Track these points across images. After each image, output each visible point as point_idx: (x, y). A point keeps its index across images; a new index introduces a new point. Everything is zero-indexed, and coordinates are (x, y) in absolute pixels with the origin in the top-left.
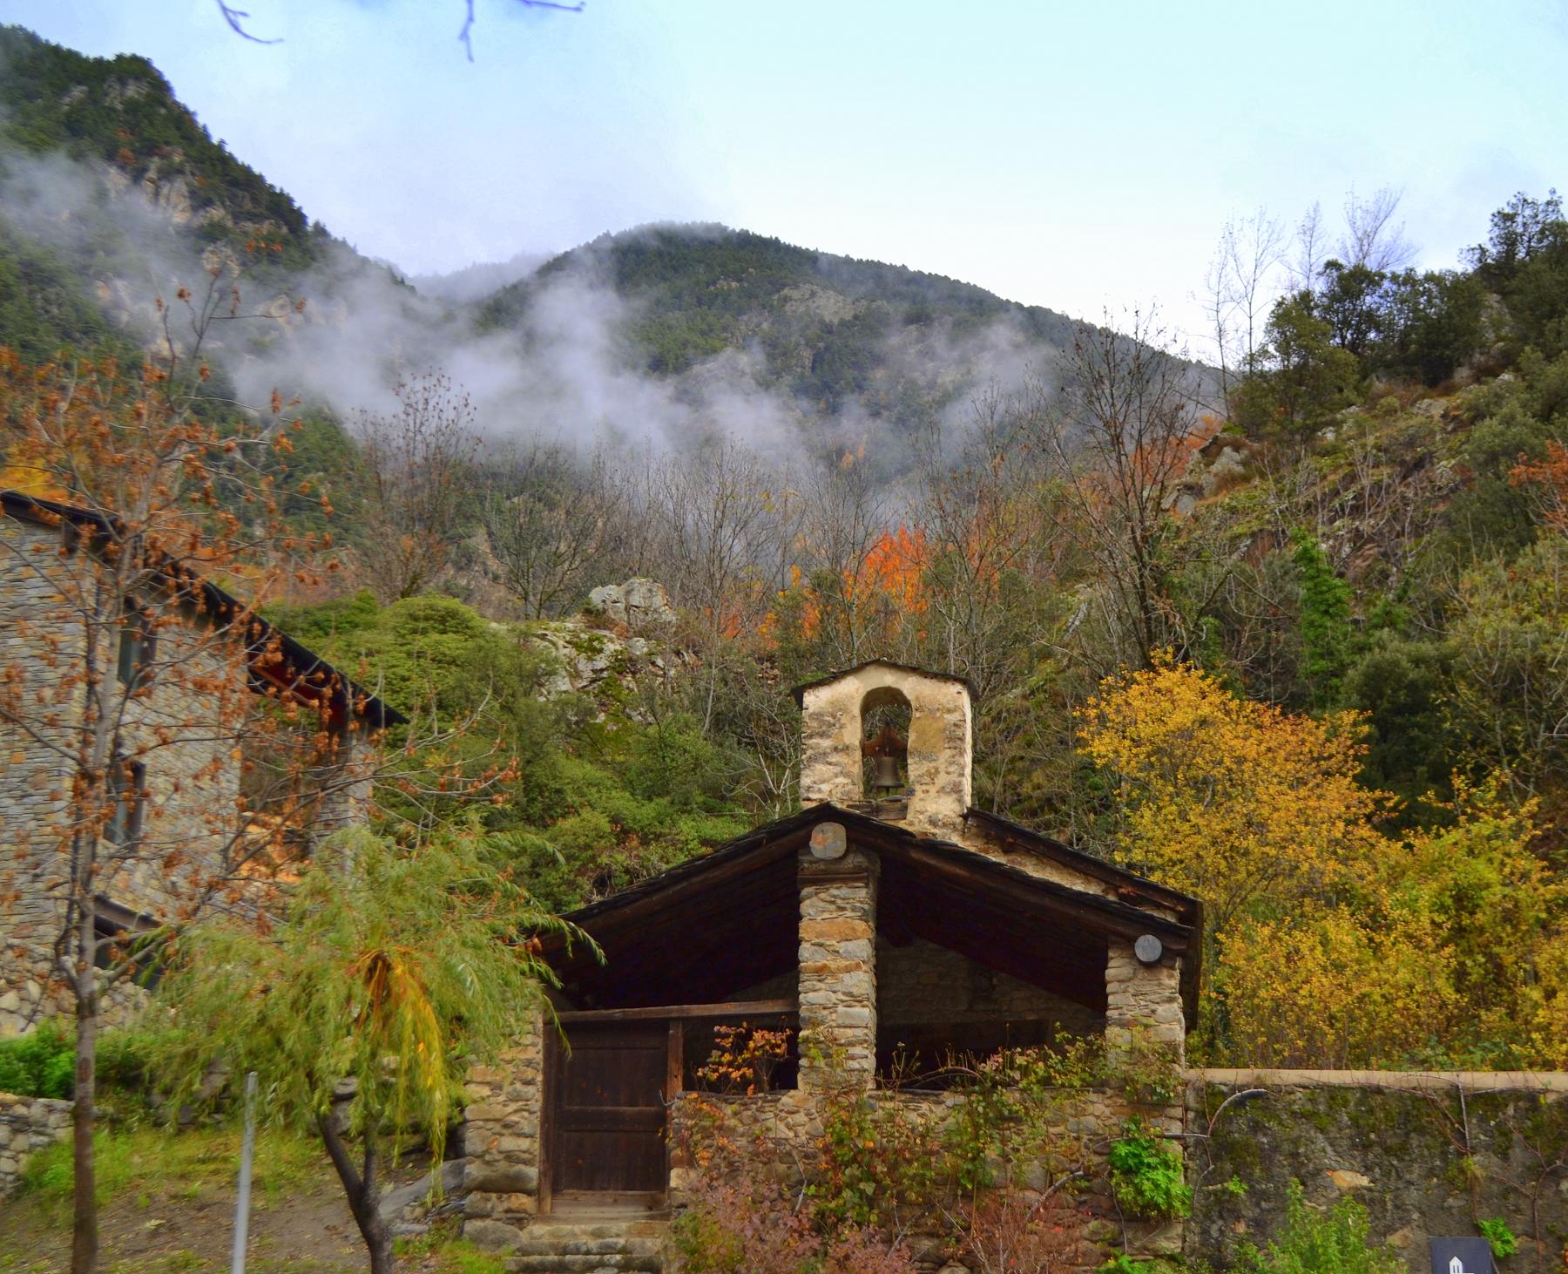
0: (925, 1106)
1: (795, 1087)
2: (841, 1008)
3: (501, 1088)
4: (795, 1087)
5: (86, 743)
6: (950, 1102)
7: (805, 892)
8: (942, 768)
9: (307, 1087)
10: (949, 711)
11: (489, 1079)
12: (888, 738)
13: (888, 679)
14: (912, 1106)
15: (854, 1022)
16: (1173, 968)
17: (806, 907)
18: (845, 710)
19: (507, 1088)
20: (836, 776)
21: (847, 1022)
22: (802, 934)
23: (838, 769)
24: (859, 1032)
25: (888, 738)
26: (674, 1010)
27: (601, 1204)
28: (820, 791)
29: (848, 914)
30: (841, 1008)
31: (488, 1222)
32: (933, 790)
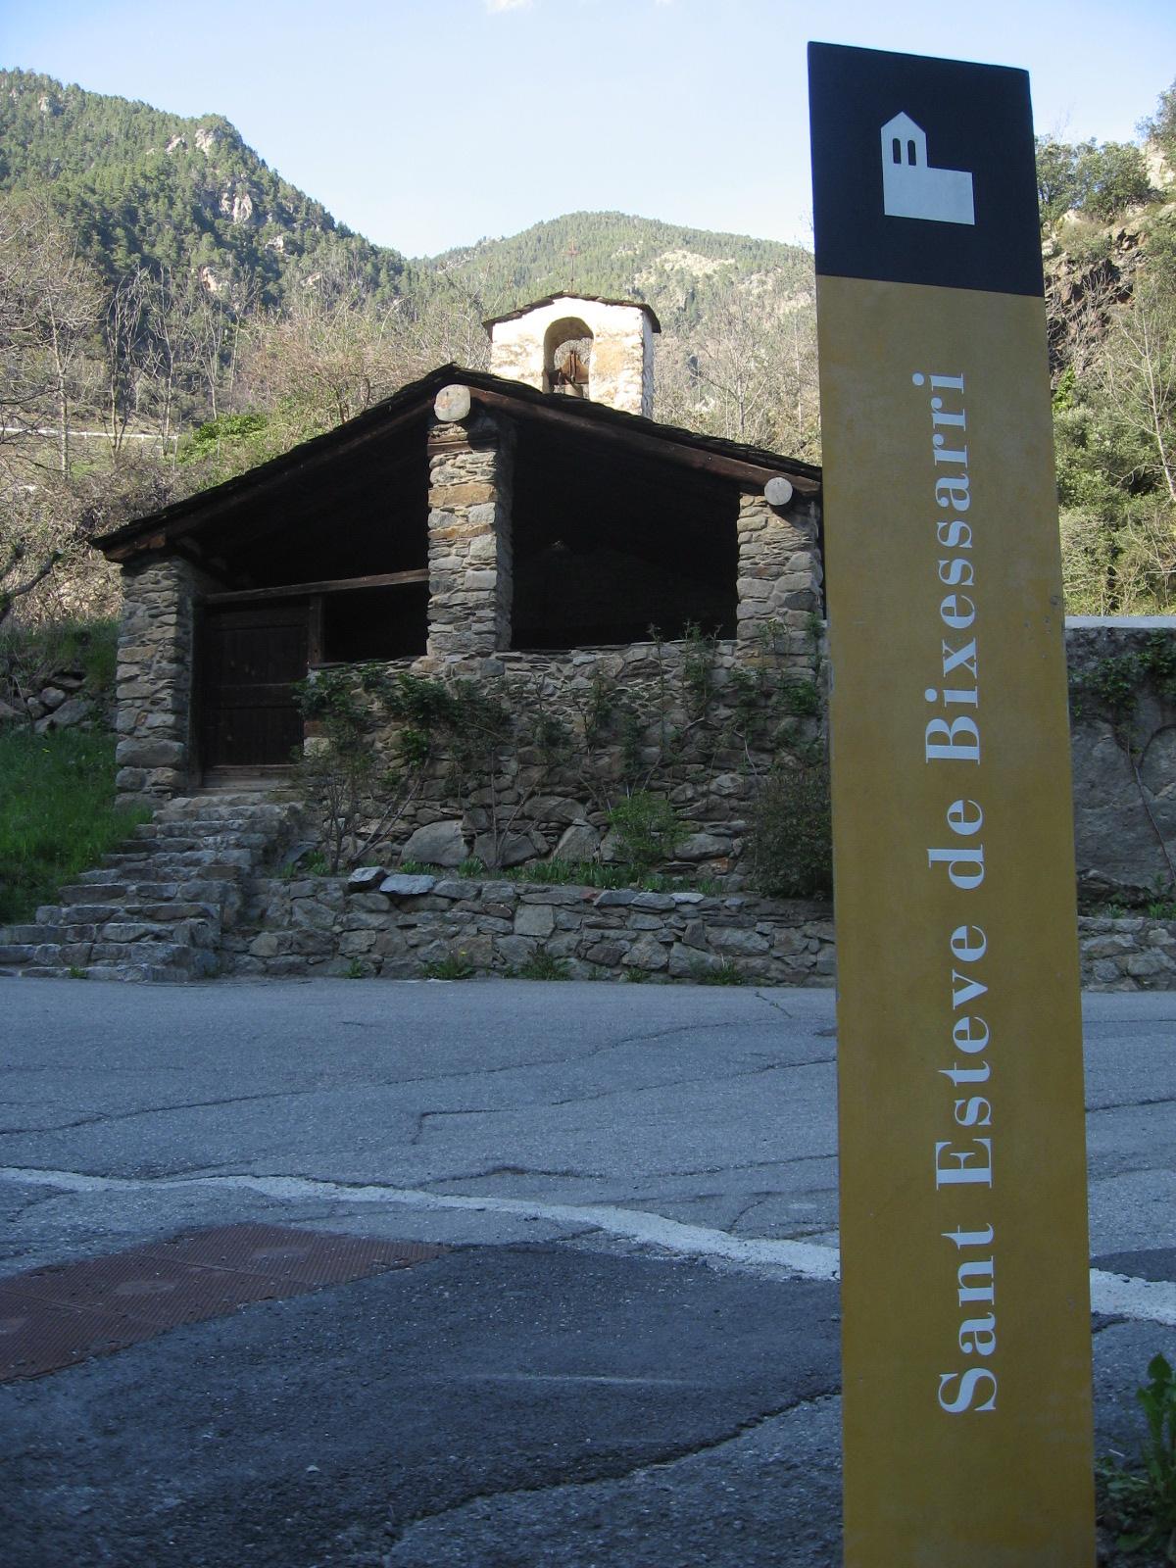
0: (553, 667)
1: (425, 653)
2: (470, 572)
3: (150, 667)
4: (425, 653)
6: (577, 661)
7: (436, 459)
8: (621, 388)
9: (755, 1190)
10: (627, 335)
11: (138, 659)
12: (973, 1281)
13: (563, 309)
15: (482, 586)
16: (807, 514)
19: (155, 666)
21: (475, 586)
22: (431, 501)
24: (484, 595)
25: (973, 1281)
26: (314, 586)
27: (251, 778)
29: (479, 477)
31: (139, 796)
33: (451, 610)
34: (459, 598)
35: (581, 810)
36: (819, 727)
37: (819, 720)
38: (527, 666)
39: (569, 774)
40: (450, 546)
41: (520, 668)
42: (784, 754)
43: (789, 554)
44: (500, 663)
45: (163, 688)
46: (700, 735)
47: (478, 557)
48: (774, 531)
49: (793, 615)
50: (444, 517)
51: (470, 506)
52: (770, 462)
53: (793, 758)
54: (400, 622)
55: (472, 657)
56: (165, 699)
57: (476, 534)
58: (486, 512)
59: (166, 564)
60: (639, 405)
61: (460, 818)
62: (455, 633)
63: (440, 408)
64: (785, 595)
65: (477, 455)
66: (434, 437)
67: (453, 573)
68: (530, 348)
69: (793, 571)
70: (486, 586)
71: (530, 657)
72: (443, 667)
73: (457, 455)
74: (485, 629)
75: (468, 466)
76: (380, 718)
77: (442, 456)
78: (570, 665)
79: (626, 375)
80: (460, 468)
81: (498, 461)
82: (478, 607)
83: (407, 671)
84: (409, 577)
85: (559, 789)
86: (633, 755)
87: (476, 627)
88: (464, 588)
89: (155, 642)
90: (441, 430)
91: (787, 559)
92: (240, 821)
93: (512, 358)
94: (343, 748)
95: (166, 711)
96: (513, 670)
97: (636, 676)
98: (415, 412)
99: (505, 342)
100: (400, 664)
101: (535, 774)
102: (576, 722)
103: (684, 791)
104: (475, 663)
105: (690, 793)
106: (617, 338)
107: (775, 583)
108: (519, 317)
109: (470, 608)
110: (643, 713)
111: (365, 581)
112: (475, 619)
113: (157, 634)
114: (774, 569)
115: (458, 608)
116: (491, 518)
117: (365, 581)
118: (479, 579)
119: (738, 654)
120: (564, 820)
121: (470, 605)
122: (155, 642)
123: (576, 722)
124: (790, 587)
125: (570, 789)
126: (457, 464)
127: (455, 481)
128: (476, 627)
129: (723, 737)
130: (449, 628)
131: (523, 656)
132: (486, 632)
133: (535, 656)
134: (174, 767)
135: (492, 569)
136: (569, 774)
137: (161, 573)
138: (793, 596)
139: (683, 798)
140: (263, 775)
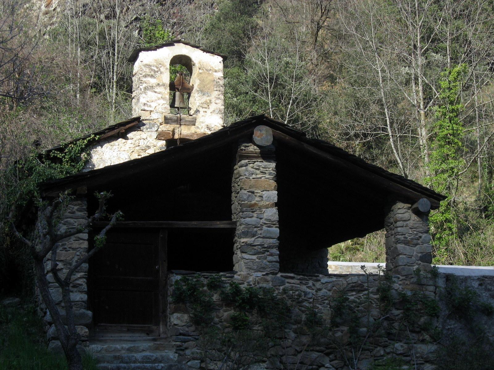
0: (310, 283)
2: (265, 228)
5: (130, 23)
8: (213, 100)
10: (216, 71)
13: (181, 49)
14: (304, 282)
17: (101, 166)
18: (163, 65)
20: (159, 99)
21: (268, 235)
23: (160, 96)
24: (271, 241)
28: (150, 106)
30: (265, 228)
32: (209, 111)
33: (255, 248)
34: (259, 241)
35: (327, 359)
36: (438, 321)
37: (438, 318)
38: (298, 282)
39: (322, 340)
40: (253, 212)
41: (292, 282)
42: (425, 334)
43: (421, 235)
44: (283, 279)
45: (80, 278)
46: (385, 324)
47: (270, 220)
48: (414, 222)
49: (423, 265)
50: (249, 195)
51: (263, 191)
52: (416, 188)
53: (428, 336)
54: (218, 252)
55: (267, 274)
56: (82, 285)
57: (267, 207)
58: (273, 195)
59: (79, 202)
60: (223, 112)
61: (264, 362)
62: (257, 260)
63: (256, 137)
64: (420, 255)
65: (265, 163)
66: (242, 150)
67: (255, 227)
68: (162, 69)
69: (423, 243)
70: (273, 236)
71: (299, 277)
72: (251, 279)
73: (255, 162)
74: (274, 260)
75: (261, 169)
76: (218, 305)
77: (246, 161)
78: (319, 283)
79: (215, 93)
80: (256, 169)
81: (277, 167)
82: (269, 247)
83: (232, 279)
84: (221, 225)
85: (318, 348)
86: (353, 331)
87: (270, 258)
88: (262, 236)
89: (73, 249)
90: (246, 147)
91: (420, 237)
92: (162, 365)
93: (153, 73)
94: (197, 321)
95: (81, 292)
96: (290, 283)
97: (352, 291)
98: (331, 158)
99: (148, 63)
100: (227, 275)
101: (305, 340)
102: (325, 312)
103: (379, 351)
104: (269, 278)
105: (382, 352)
106: (211, 72)
107: (415, 248)
108: (155, 50)
109: (265, 248)
110: (357, 310)
111: (194, 224)
112: (268, 253)
113: (75, 245)
114: (415, 241)
115: (259, 247)
116: (276, 200)
117: (194, 224)
118: (268, 232)
119: (400, 282)
120: (320, 365)
121: (266, 246)
122: (73, 249)
123: (325, 312)
124: (422, 251)
125: (322, 348)
126: (255, 167)
127: (254, 176)
128: (270, 258)
129: (396, 325)
130: (254, 257)
131: (295, 276)
132: (274, 262)
133: (301, 276)
134: (87, 326)
135: (276, 227)
136: (322, 340)
137: (76, 208)
138: (423, 255)
139: (378, 355)
140: (129, 331)
